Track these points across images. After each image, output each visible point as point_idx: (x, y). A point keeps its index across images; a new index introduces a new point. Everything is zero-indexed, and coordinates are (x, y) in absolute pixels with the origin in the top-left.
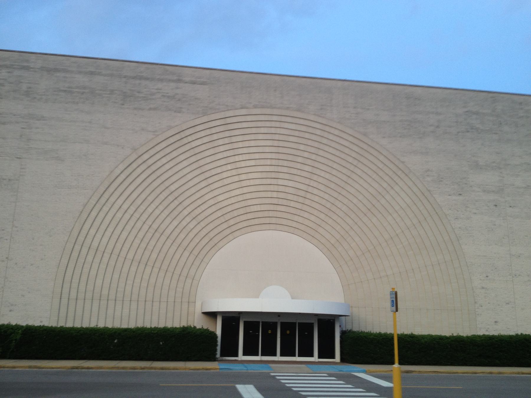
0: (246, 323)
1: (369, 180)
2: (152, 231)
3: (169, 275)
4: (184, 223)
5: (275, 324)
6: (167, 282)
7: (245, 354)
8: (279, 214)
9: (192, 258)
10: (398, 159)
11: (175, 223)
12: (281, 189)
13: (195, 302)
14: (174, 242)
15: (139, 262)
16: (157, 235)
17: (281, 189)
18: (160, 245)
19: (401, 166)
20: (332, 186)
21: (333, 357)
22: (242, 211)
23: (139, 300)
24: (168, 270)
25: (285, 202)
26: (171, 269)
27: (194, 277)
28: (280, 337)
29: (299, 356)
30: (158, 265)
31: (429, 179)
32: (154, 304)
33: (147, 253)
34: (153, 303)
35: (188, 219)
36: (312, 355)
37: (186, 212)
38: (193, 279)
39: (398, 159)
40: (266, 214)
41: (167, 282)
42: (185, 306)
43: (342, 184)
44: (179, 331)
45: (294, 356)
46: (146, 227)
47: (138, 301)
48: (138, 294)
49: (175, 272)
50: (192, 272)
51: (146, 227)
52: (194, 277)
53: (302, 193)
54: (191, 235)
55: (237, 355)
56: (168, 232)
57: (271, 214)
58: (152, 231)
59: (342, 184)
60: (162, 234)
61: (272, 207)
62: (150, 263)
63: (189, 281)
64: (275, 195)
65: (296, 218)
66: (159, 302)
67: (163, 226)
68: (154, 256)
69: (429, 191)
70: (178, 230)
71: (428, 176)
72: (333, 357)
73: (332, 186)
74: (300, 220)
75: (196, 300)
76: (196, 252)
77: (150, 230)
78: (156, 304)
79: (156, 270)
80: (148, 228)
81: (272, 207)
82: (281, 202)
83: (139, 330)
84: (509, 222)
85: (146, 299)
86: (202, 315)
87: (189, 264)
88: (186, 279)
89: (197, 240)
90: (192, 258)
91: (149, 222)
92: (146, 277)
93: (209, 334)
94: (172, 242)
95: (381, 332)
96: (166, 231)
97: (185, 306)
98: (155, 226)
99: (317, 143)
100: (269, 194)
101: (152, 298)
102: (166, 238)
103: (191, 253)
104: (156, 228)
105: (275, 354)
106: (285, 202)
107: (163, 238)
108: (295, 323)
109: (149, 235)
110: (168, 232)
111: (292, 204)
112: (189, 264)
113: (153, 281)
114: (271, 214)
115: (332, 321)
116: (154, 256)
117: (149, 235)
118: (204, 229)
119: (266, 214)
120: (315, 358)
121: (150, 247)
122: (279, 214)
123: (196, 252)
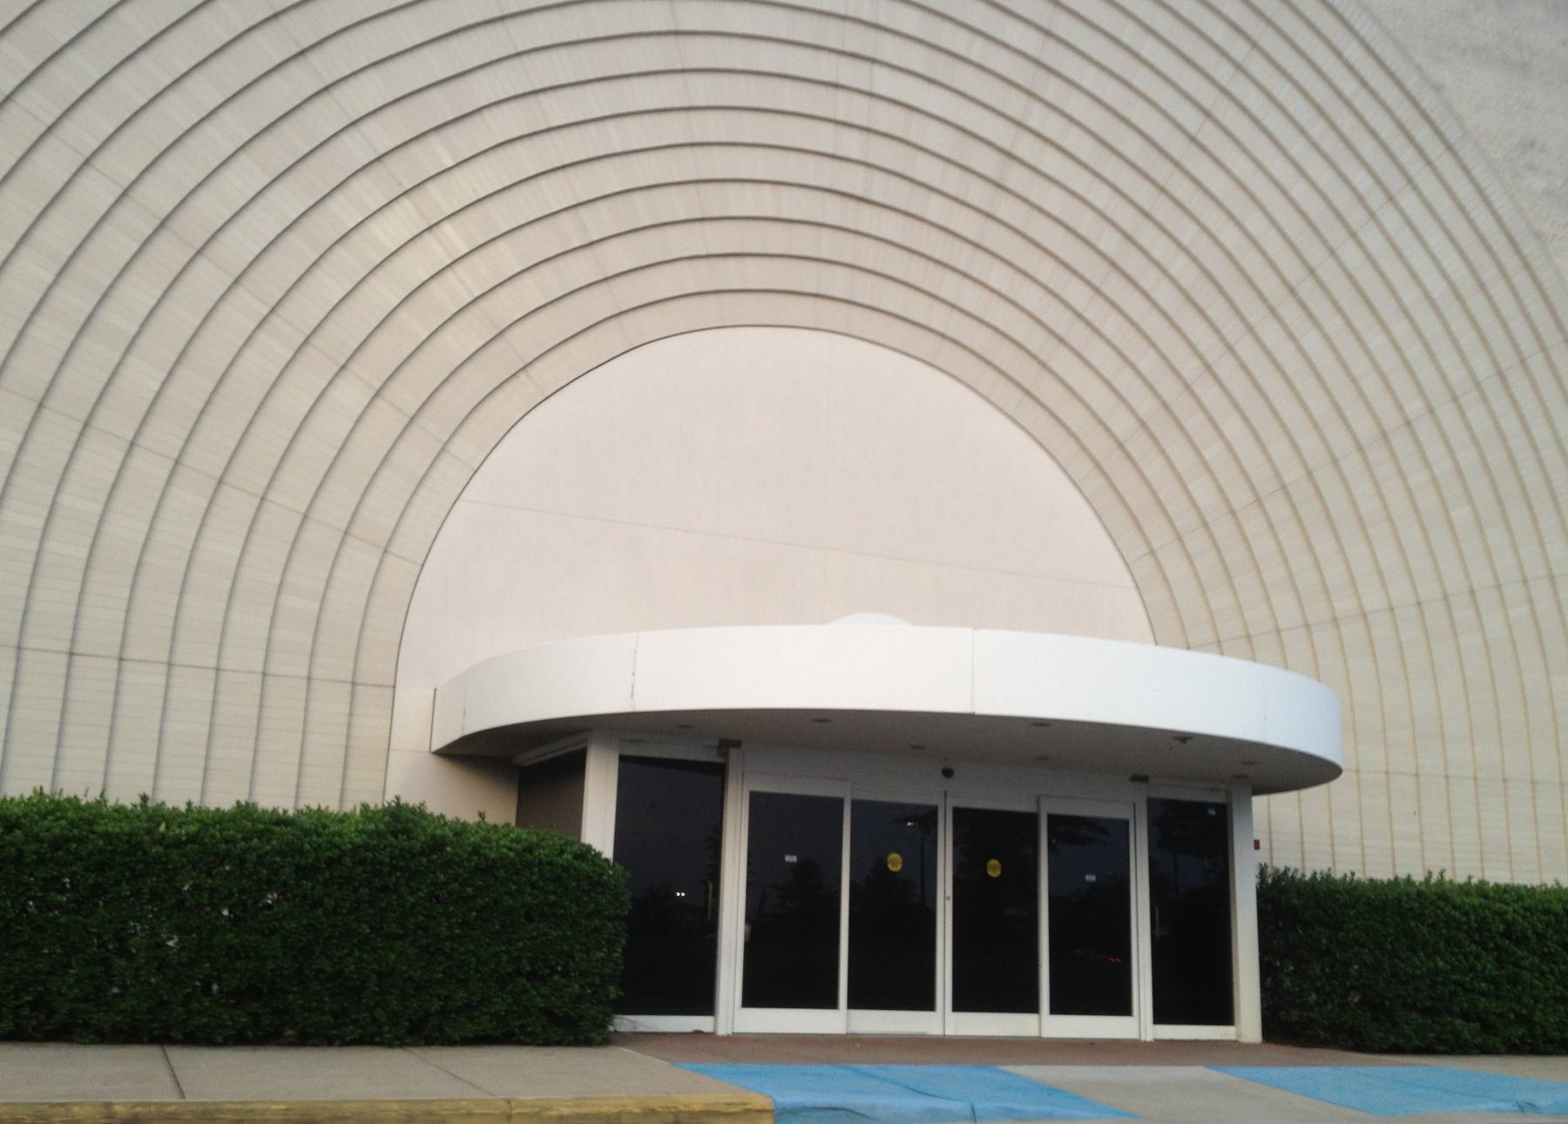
0: (761, 806)
1: (1298, 147)
2: (134, 222)
3: (234, 505)
4: (343, 212)
5: (926, 819)
6: (221, 546)
7: (754, 996)
8: (868, 254)
9: (385, 421)
10: (1418, 68)
11: (288, 201)
12: (887, 118)
13: (394, 687)
14: (273, 310)
15: (41, 406)
16: (169, 253)
17: (887, 118)
18: (182, 313)
19: (1428, 101)
20: (1131, 146)
21: (1223, 1013)
22: (677, 204)
23: (30, 642)
24: (232, 479)
25: (898, 194)
26: (251, 473)
27: (390, 541)
28: (950, 892)
29: (1060, 1006)
30: (165, 433)
31: (1537, 183)
32: (131, 676)
33: (96, 357)
34: (120, 670)
35: (369, 192)
36: (1121, 1006)
37: (356, 149)
38: (386, 551)
39: (1418, 68)
40: (802, 241)
41: (221, 546)
42: (330, 706)
43: (1177, 146)
44: (361, 832)
45: (1032, 1007)
46: (96, 192)
47: (19, 648)
48: (21, 605)
49: (272, 495)
50: (381, 508)
51: (96, 192)
52: (390, 541)
53: (985, 161)
54: (384, 292)
55: (704, 1003)
56: (241, 243)
57: (827, 244)
58: (134, 222)
59: (1177, 146)
60: (199, 252)
61: (833, 211)
62: (118, 419)
63: (361, 559)
64: (852, 144)
65: (950, 286)
66: (163, 669)
67: (211, 208)
68: (142, 376)
69: (1538, 235)
70: (301, 249)
71: (1531, 167)
72: (1223, 1013)
73: (1131, 146)
74: (971, 298)
75: (399, 679)
76: (406, 393)
77: (124, 213)
78: (143, 681)
79: (149, 468)
80: (112, 200)
81: (833, 211)
82: (879, 187)
83: (52, 812)
84: (434, 823)
85: (73, 641)
86: (437, 763)
87: (364, 454)
88: (342, 543)
89: (414, 324)
90: (385, 421)
91: (123, 162)
92: (80, 502)
93: (576, 857)
94: (266, 310)
95: (1487, 879)
96: (226, 239)
97: (330, 706)
98: (159, 195)
99: (922, 51)
100: (825, 137)
101: (117, 640)
102: (229, 281)
103: (378, 394)
104: (91, 444)
105: (923, 1000)
106: (898, 194)
107: (207, 279)
108: (1033, 818)
109: (116, 244)
110: (241, 243)
111: (935, 208)
112: (364, 454)
113: (127, 527)
114: (827, 244)
115: (1212, 812)
116: (142, 376)
117: (116, 244)
118: (459, 268)
119: (802, 241)
120: (1139, 1024)
121: (120, 319)
122: (868, 254)
123: (406, 393)
